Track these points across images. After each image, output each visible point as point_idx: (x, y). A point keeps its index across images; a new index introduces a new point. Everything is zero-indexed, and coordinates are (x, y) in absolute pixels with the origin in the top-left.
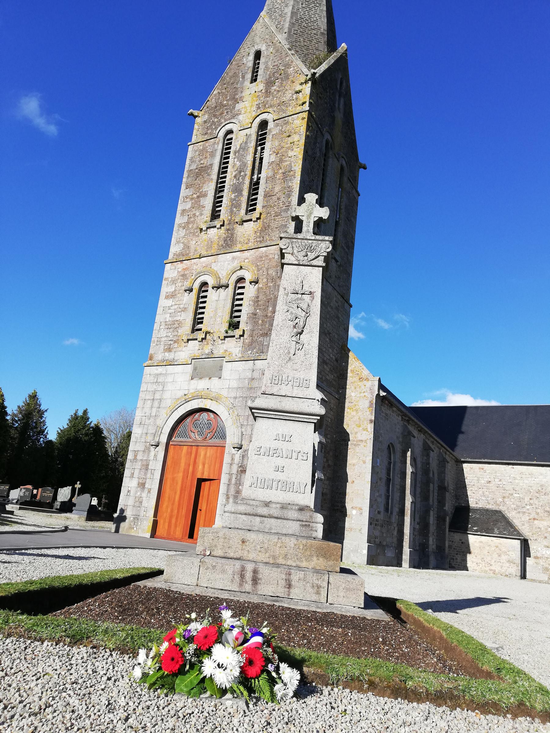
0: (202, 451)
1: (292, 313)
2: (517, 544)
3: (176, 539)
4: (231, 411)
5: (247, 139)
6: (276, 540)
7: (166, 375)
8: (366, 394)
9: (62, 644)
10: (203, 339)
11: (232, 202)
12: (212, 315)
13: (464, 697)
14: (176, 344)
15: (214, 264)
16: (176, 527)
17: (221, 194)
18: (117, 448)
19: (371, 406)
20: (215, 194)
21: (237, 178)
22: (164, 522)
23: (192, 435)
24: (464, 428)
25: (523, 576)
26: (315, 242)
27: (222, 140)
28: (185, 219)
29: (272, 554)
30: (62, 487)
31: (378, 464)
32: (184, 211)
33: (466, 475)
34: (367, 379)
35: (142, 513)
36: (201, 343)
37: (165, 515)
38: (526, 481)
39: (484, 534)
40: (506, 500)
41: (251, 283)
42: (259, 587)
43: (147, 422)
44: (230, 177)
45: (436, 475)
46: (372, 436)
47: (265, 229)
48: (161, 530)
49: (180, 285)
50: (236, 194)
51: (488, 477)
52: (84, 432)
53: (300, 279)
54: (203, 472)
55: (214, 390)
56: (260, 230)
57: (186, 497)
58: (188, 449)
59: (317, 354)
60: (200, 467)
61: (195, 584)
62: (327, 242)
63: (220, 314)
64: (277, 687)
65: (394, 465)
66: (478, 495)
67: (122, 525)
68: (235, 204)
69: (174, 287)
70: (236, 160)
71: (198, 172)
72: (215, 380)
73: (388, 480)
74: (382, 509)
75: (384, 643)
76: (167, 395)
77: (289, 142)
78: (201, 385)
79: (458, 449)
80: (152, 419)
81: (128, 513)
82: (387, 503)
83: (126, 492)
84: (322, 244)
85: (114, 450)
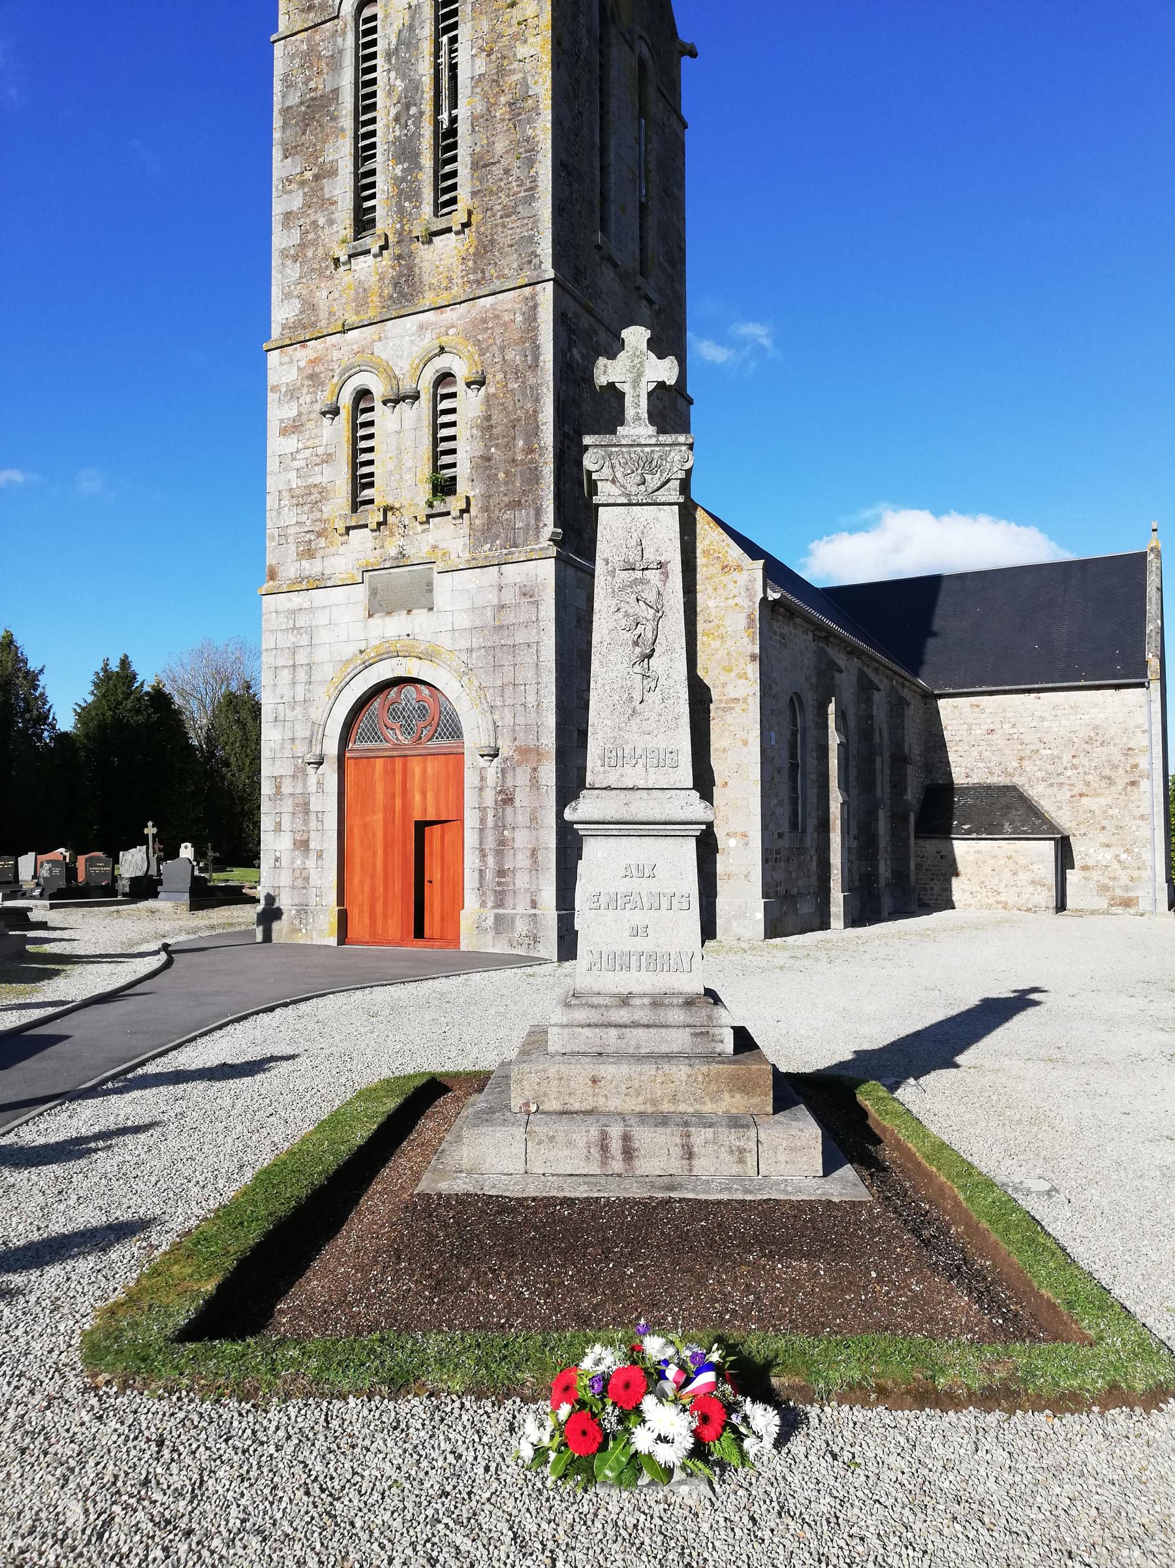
0: (416, 767)
1: (627, 615)
2: (1047, 848)
3: (389, 943)
4: (465, 679)
5: (412, 18)
6: (653, 1072)
7: (311, 610)
8: (738, 600)
9: (377, 1398)
10: (379, 524)
11: (398, 187)
12: (391, 467)
13: (1026, 1391)
14: (322, 540)
15: (378, 344)
16: (385, 917)
17: (368, 166)
18: (209, 730)
19: (750, 626)
20: (356, 167)
21: (403, 121)
22: (361, 912)
23: (390, 734)
24: (937, 624)
25: (1061, 906)
26: (657, 449)
27: (353, 24)
28: (295, 237)
29: (648, 1096)
30: (126, 849)
31: (773, 743)
32: (288, 215)
33: (944, 721)
34: (739, 568)
35: (313, 900)
36: (377, 533)
37: (360, 898)
38: (1064, 722)
39: (984, 836)
40: (1025, 763)
41: (469, 385)
42: (637, 1163)
43: (290, 715)
44: (385, 122)
45: (886, 735)
46: (757, 687)
47: (484, 250)
48: (356, 928)
49: (308, 400)
50: (406, 165)
51: (989, 721)
52: (129, 704)
53: (635, 535)
54: (424, 807)
55: (421, 637)
56: (474, 254)
57: (397, 859)
58: (385, 764)
59: (686, 696)
60: (418, 798)
61: (522, 1171)
62: (684, 448)
63: (410, 464)
64: (747, 1444)
65: (803, 736)
66: (970, 759)
67: (276, 926)
68: (406, 192)
69: (294, 405)
70: (393, 75)
71: (306, 113)
72: (420, 614)
73: (794, 767)
74: (785, 827)
75: (880, 1280)
76: (321, 655)
77: (514, 22)
78: (393, 627)
79: (926, 669)
80: (299, 709)
81: (284, 902)
82: (795, 813)
83: (272, 861)
84: (673, 454)
85: (203, 734)
